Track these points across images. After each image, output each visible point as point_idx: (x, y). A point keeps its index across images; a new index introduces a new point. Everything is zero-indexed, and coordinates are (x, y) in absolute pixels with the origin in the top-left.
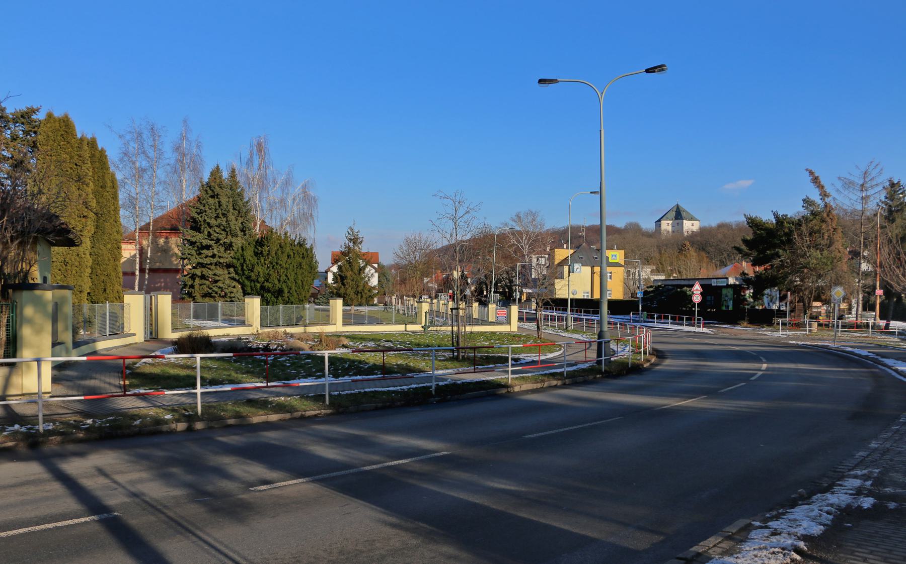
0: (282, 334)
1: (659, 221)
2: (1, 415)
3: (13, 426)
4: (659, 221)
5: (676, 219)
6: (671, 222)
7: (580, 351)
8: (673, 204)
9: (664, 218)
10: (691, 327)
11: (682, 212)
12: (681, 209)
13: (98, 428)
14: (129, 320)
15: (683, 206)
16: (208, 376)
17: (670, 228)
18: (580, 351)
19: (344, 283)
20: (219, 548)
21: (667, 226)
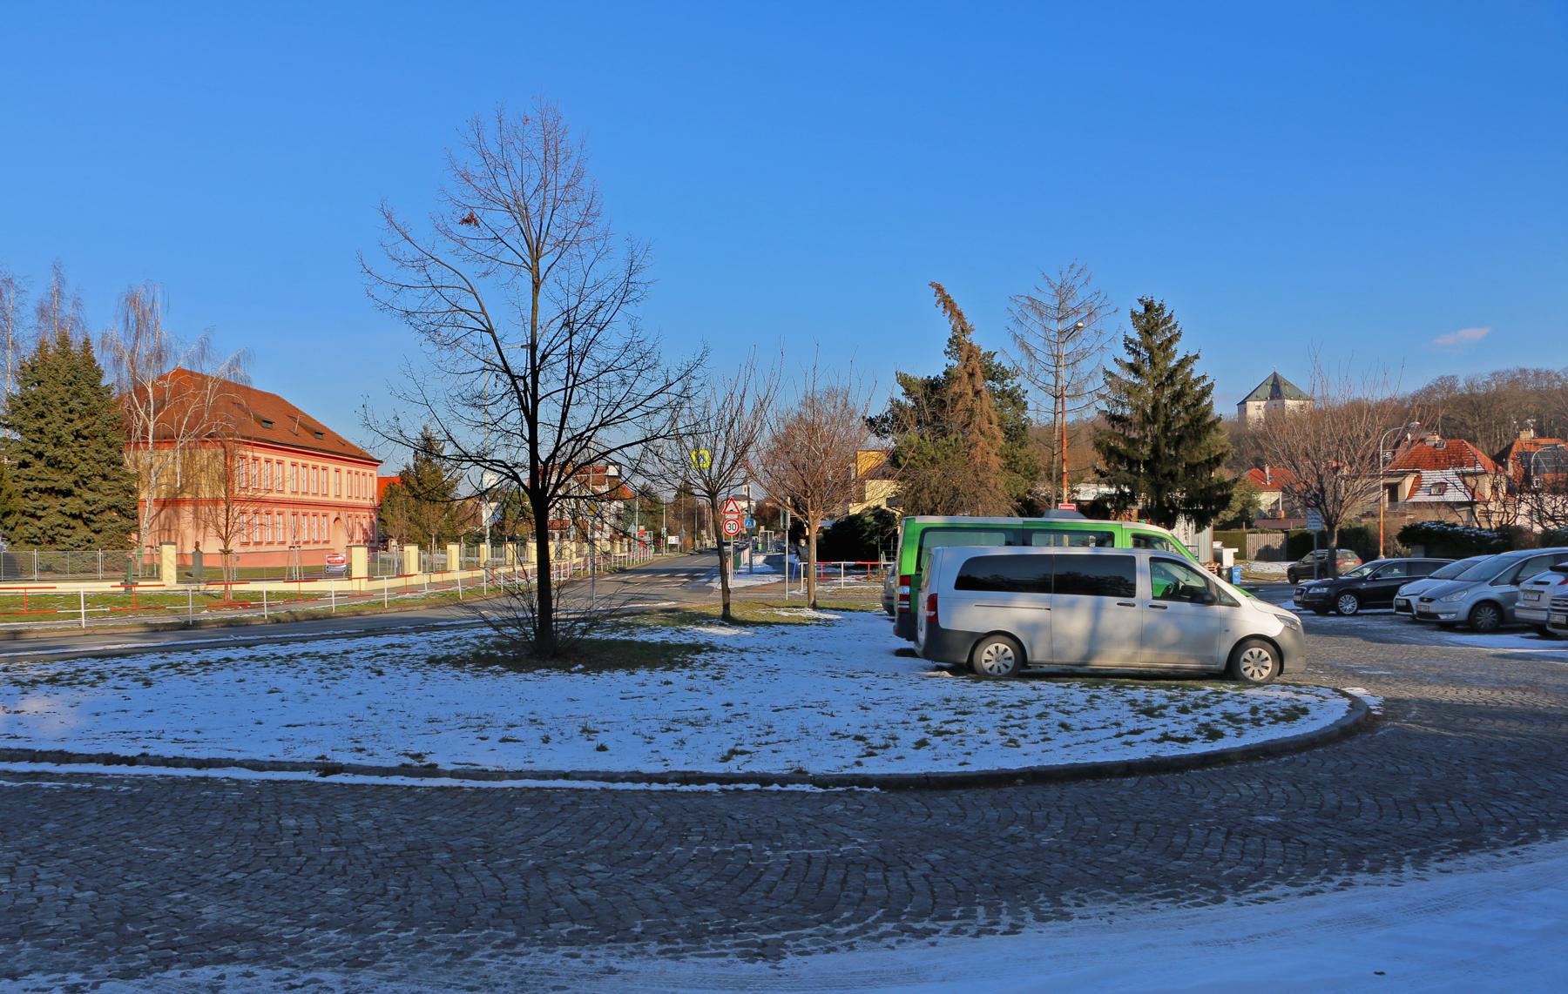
0: (1108, 427)
1: (1244, 402)
2: (1566, 832)
3: (650, 784)
4: (1244, 402)
5: (1272, 398)
6: (1263, 404)
7: (783, 624)
8: (1264, 375)
9: (1253, 396)
10: (130, 755)
11: (1282, 387)
12: (1279, 379)
13: (1498, 529)
14: (566, 776)
15: (1286, 375)
16: (838, 570)
17: (1261, 414)
18: (783, 624)
19: (718, 543)
20: (1505, 703)
21: (1256, 410)
